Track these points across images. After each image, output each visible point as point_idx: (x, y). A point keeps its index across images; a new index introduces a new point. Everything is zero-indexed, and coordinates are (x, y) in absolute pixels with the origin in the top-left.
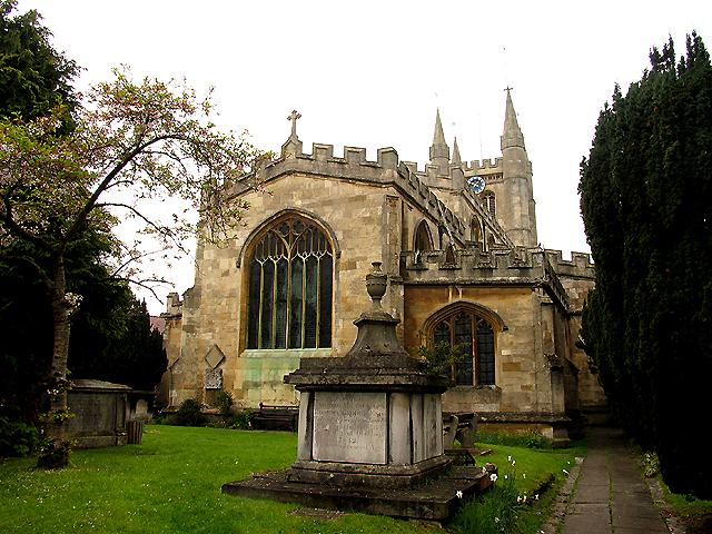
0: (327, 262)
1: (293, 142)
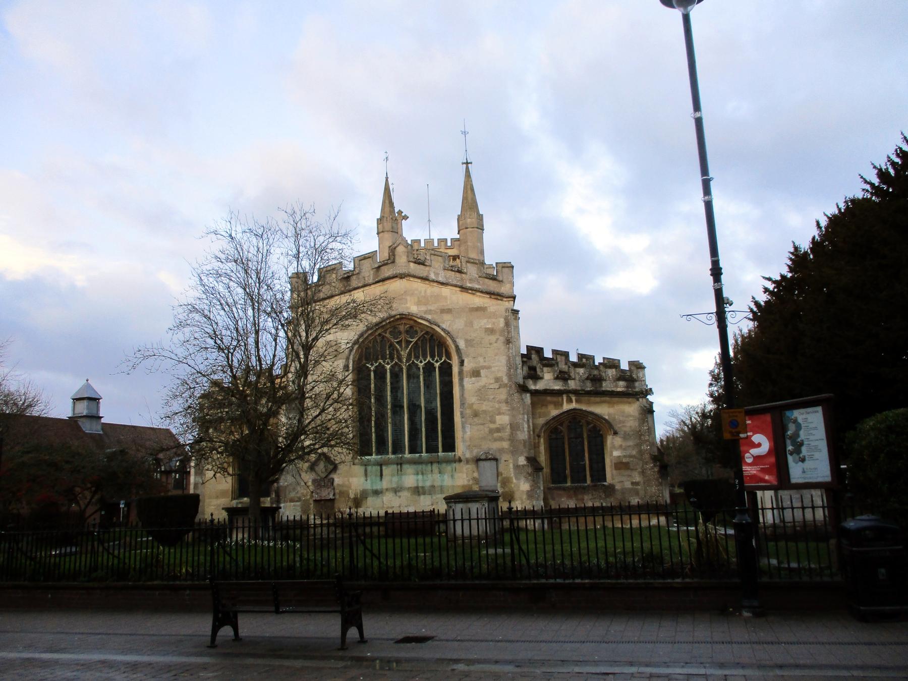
0: (446, 370)
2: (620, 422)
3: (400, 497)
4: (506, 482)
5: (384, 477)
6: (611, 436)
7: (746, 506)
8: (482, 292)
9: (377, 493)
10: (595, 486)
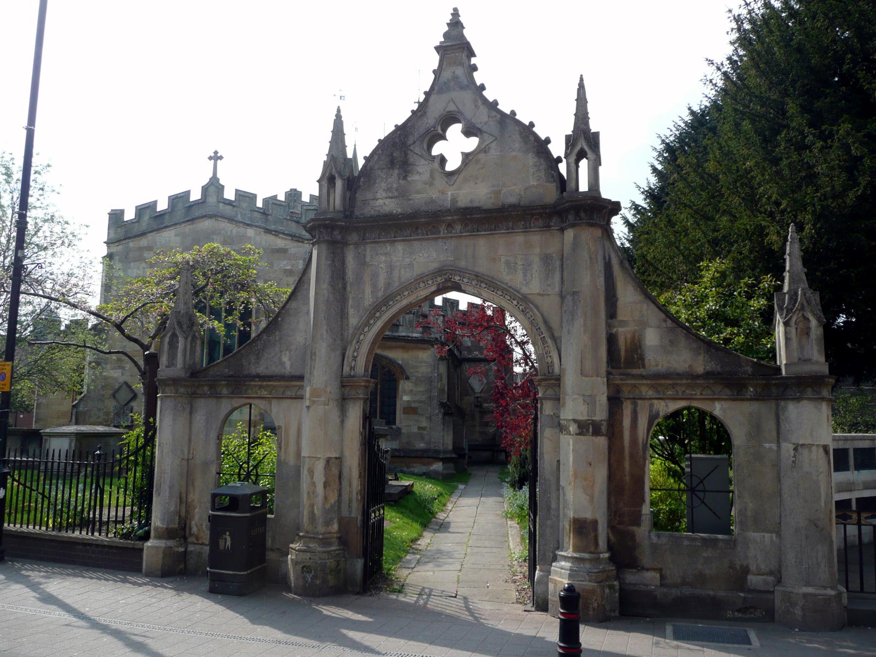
1: (214, 186)
7: (781, 374)
8: (284, 234)
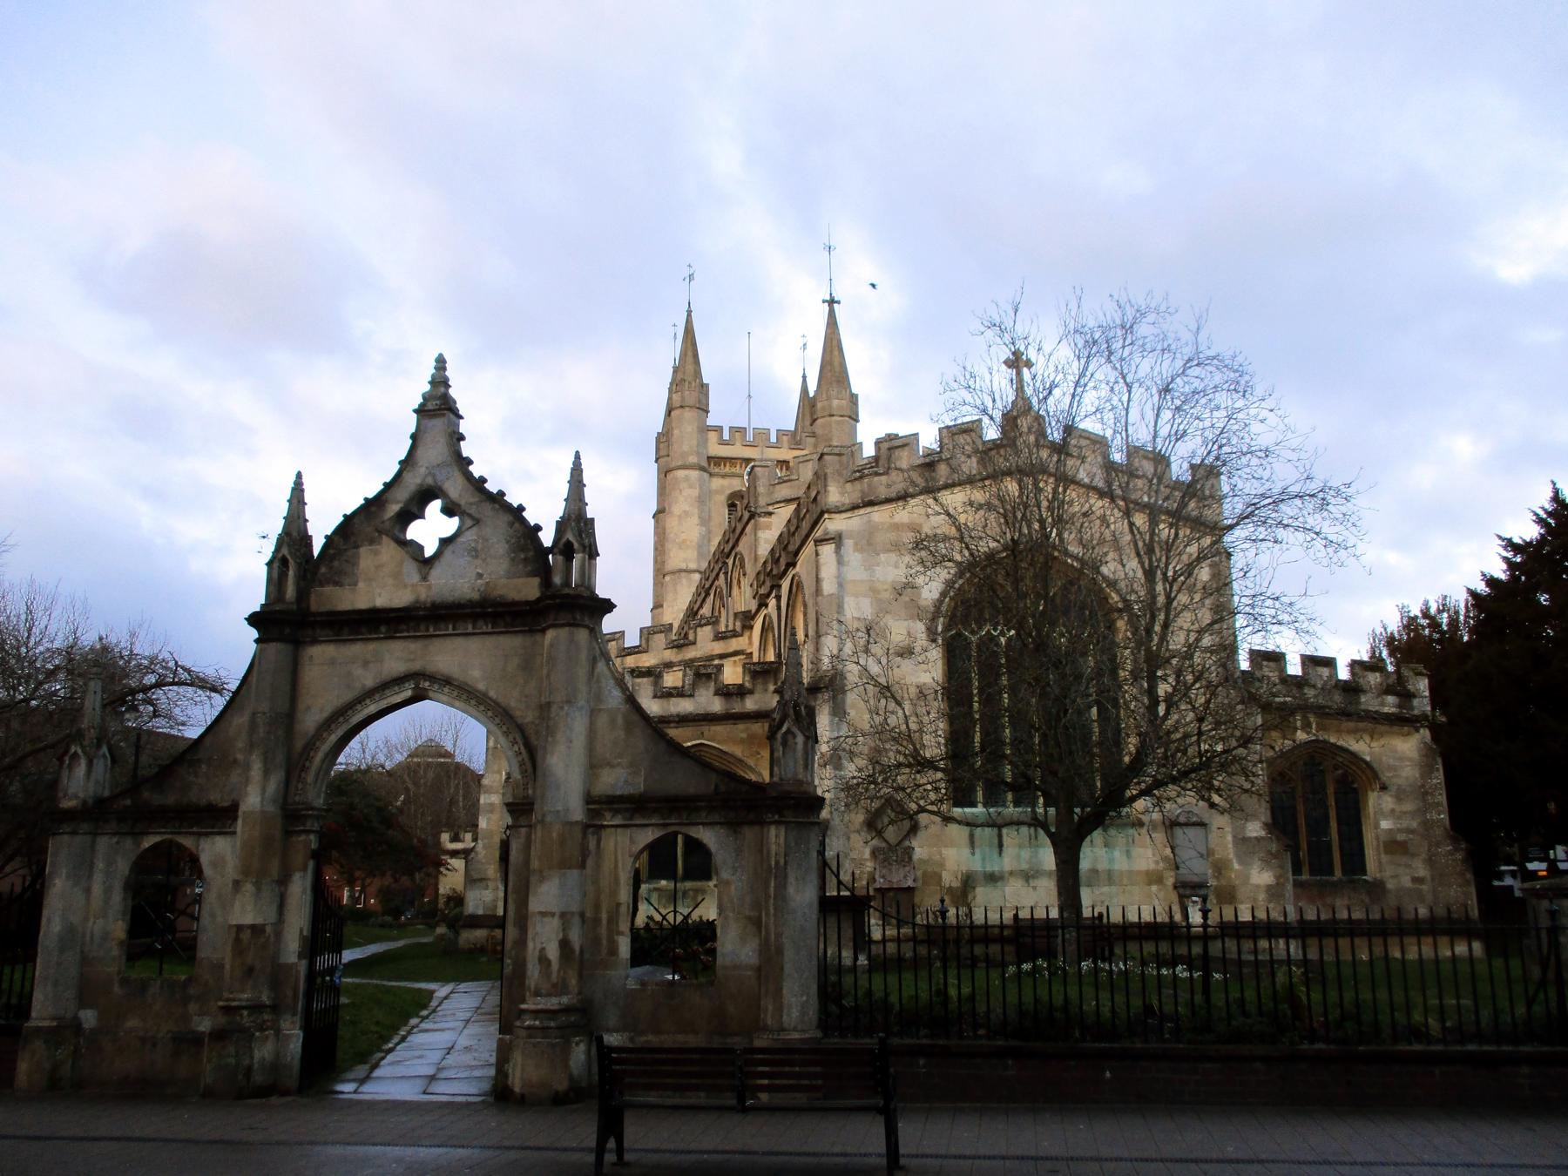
2: (1392, 768)
3: (1035, 888)
4: (1220, 868)
5: (1004, 849)
6: (1376, 793)
9: (993, 878)
10: (1352, 881)
